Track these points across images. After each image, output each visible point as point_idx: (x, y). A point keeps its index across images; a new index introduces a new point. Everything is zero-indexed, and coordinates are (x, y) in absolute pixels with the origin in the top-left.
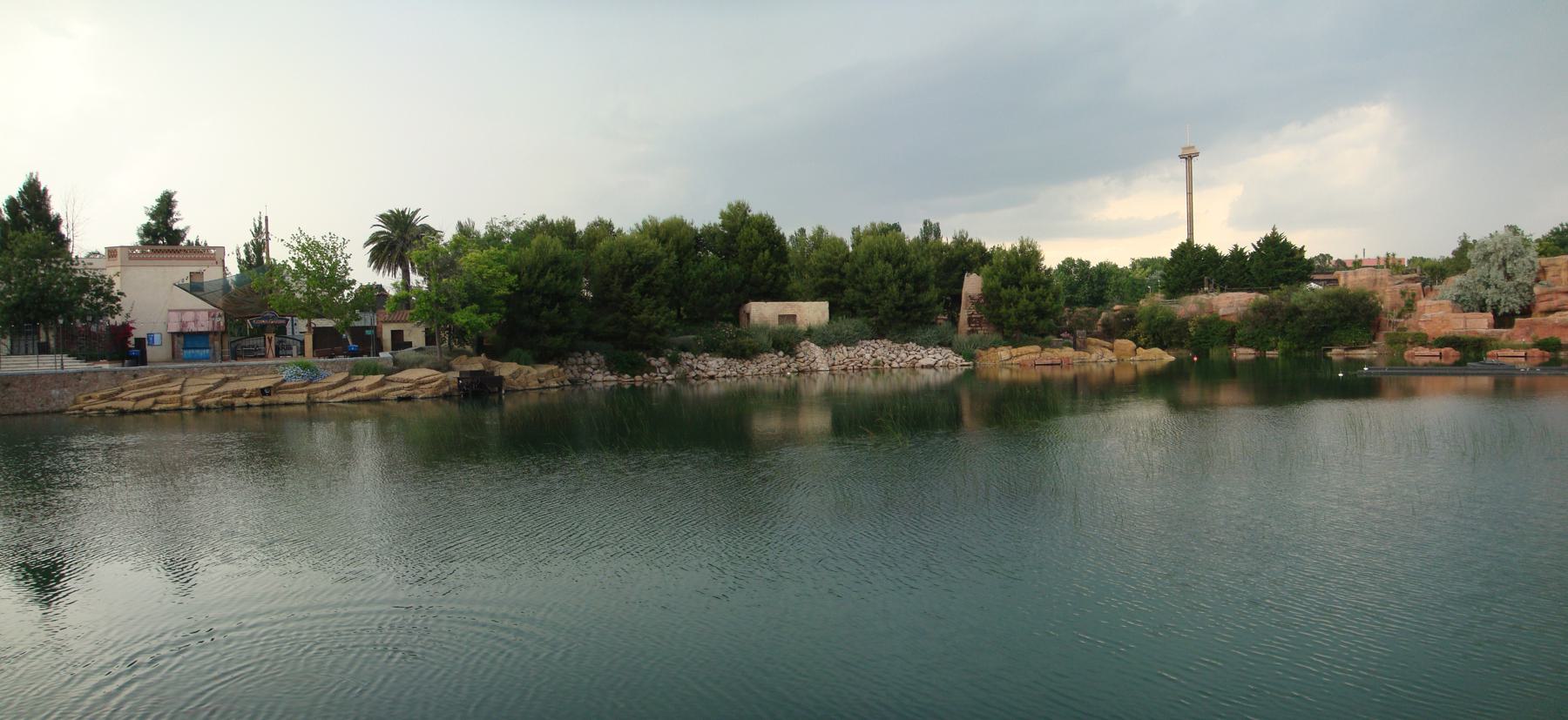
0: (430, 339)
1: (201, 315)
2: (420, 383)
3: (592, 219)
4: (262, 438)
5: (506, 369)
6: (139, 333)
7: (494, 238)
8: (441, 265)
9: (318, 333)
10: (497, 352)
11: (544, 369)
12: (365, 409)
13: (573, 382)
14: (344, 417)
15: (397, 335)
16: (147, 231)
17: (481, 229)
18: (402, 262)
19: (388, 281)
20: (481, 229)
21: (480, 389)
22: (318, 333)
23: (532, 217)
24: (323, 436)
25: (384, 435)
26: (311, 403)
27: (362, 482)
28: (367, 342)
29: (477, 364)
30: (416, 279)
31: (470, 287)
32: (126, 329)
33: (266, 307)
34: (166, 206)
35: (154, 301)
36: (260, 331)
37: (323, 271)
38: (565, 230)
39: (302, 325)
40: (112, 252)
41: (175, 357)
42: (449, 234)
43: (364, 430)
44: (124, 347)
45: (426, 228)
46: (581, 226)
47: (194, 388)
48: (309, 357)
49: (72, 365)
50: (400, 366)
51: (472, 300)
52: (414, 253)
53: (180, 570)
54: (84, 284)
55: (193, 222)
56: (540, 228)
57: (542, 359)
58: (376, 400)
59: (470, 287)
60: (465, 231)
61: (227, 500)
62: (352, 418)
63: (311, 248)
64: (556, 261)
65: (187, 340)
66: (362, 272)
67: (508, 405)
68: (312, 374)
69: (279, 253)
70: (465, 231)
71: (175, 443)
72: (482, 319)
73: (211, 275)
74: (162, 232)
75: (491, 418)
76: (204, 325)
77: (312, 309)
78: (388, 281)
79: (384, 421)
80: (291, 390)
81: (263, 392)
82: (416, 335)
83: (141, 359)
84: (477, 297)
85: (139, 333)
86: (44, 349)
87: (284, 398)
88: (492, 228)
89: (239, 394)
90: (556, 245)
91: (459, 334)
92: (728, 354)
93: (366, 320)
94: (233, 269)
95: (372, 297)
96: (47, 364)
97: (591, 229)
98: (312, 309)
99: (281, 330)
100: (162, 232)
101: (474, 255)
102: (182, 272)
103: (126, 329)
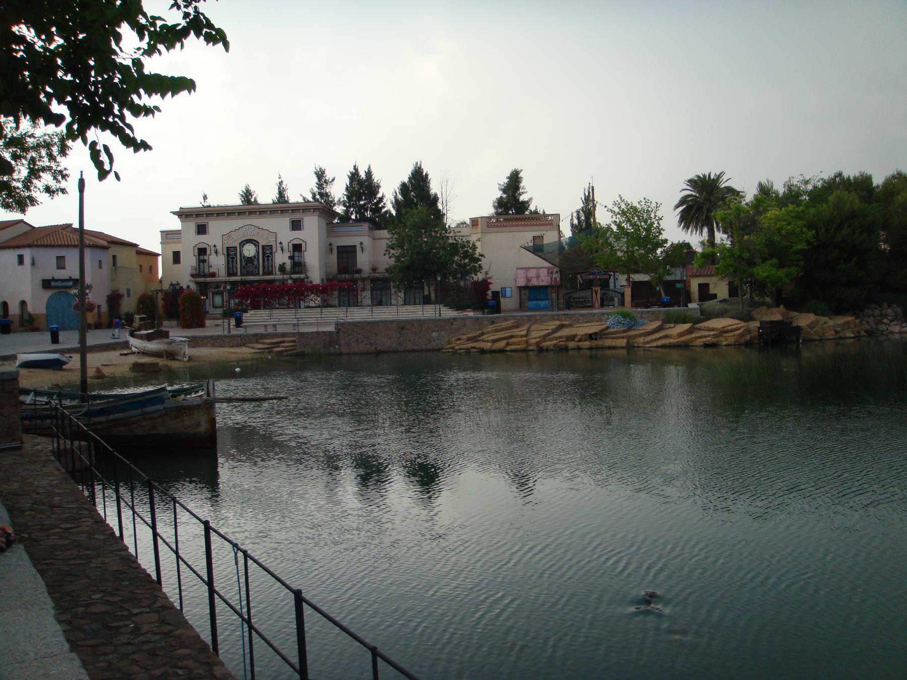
0: (733, 291)
1: (541, 272)
2: (723, 331)
3: (890, 172)
4: (589, 374)
5: (804, 320)
6: (495, 287)
7: (792, 195)
8: (744, 221)
9: (637, 287)
10: (796, 304)
11: (841, 320)
12: (675, 354)
13: (870, 333)
14: (658, 360)
15: (703, 288)
16: (501, 204)
17: (780, 188)
18: (708, 222)
19: (695, 239)
20: (780, 188)
21: (778, 338)
22: (637, 287)
23: (828, 174)
24: (639, 376)
25: (691, 378)
26: (630, 347)
27: (674, 419)
28: (677, 294)
29: (776, 315)
30: (720, 237)
31: (770, 243)
32: (485, 284)
33: (598, 263)
34: (514, 181)
35: (507, 262)
36: (588, 285)
37: (639, 228)
38: (864, 182)
39: (622, 279)
40: (474, 222)
41: (522, 307)
42: (750, 194)
43: (674, 374)
44: (483, 298)
45: (730, 190)
46: (878, 180)
47: (536, 334)
48: (628, 308)
49: (448, 313)
50: (707, 316)
51: (771, 255)
52: (719, 213)
53: (522, 481)
54: (455, 248)
55: (537, 196)
56: (837, 185)
57: (838, 310)
58: (685, 346)
59: (770, 243)
60: (765, 190)
61: (562, 426)
62: (665, 362)
63: (629, 212)
64: (853, 215)
65: (531, 293)
66: (673, 232)
67: (806, 354)
68: (631, 322)
69: (603, 218)
70: (765, 190)
71: (519, 376)
72: (781, 273)
73: (549, 238)
74: (512, 204)
75: (788, 366)
76: (544, 280)
77: (631, 265)
78: (695, 239)
79: (691, 364)
80: (612, 335)
81: (591, 337)
82: (721, 289)
83: (497, 309)
84: (776, 251)
85: (495, 287)
86: (427, 301)
87: (608, 342)
88: (790, 187)
89: (572, 338)
90: (853, 200)
91: (759, 286)
93: (677, 274)
94: (567, 232)
95: (682, 252)
96: (428, 312)
97: (889, 182)
98: (631, 265)
99: (605, 284)
100: (512, 204)
101: (773, 213)
102: (526, 236)
103: (485, 284)
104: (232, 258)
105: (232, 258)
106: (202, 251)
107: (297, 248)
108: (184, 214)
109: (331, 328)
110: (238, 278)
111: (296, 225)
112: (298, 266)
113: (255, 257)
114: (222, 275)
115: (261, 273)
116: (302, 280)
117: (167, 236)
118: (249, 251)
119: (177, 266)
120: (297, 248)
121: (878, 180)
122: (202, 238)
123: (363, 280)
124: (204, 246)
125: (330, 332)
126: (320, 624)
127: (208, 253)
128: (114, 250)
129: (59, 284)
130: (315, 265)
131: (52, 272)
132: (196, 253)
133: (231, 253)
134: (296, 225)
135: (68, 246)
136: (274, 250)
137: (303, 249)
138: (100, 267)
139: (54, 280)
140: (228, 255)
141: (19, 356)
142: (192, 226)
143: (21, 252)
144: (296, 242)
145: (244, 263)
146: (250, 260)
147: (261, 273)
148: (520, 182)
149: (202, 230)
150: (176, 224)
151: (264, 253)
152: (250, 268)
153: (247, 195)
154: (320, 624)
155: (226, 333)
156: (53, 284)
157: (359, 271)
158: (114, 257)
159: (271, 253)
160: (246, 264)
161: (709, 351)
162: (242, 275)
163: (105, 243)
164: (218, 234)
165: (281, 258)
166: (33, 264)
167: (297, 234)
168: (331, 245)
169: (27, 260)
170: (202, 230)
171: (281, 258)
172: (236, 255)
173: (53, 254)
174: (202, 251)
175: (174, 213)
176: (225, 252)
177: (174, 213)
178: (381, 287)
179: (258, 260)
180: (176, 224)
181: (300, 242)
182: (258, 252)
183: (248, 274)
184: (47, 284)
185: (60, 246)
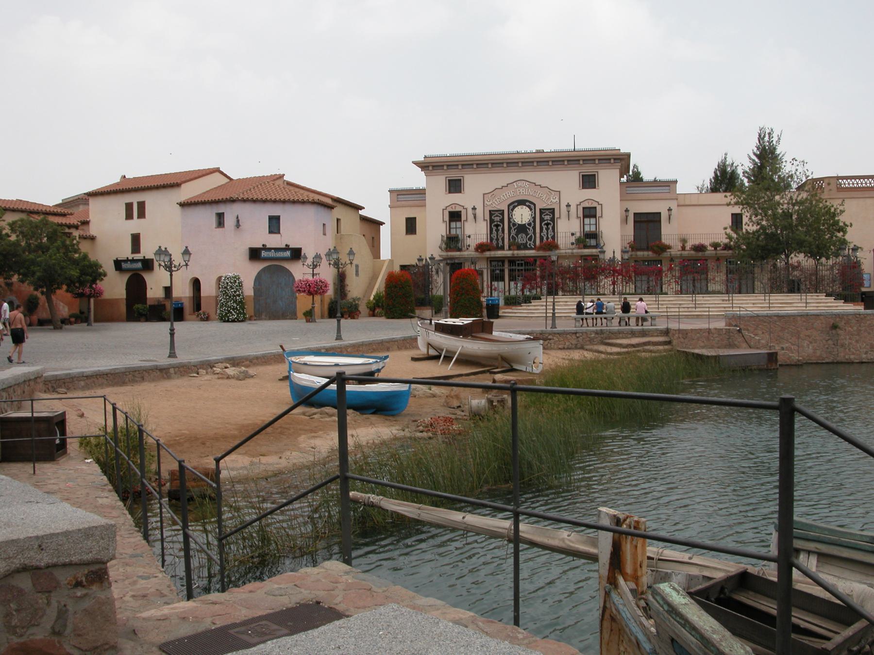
53: (182, 467)
92: (73, 504)
104: (497, 226)
105: (497, 226)
106: (455, 216)
107: (590, 213)
108: (429, 166)
109: (721, 325)
110: (507, 253)
111: (589, 182)
112: (590, 238)
113: (529, 224)
115: (506, 247)
116: (595, 258)
117: (401, 197)
118: (522, 215)
119: (411, 237)
120: (590, 213)
122: (455, 198)
123: (672, 259)
124: (458, 209)
125: (719, 330)
126: (171, 551)
127: (463, 218)
128: (339, 212)
129: (272, 254)
130: (615, 237)
131: (261, 237)
132: (447, 218)
133: (496, 219)
134: (589, 182)
135: (284, 202)
136: (557, 215)
138: (325, 234)
139: (265, 248)
140: (492, 221)
142: (440, 181)
143: (221, 209)
144: (586, 205)
145: (513, 233)
146: (522, 229)
147: (506, 247)
149: (455, 186)
150: (418, 179)
151: (542, 220)
152: (521, 239)
154: (171, 551)
155: (549, 329)
156: (264, 254)
157: (666, 248)
158: (338, 220)
159: (553, 219)
162: (510, 249)
163: (329, 201)
164: (477, 193)
166: (238, 225)
167: (589, 193)
168: (627, 211)
169: (229, 221)
170: (455, 186)
171: (567, 229)
172: (502, 221)
173: (265, 212)
174: (455, 216)
175: (415, 163)
176: (487, 217)
178: (695, 269)
179: (534, 228)
180: (418, 179)
182: (534, 218)
183: (519, 247)
184: (255, 254)
185: (275, 202)
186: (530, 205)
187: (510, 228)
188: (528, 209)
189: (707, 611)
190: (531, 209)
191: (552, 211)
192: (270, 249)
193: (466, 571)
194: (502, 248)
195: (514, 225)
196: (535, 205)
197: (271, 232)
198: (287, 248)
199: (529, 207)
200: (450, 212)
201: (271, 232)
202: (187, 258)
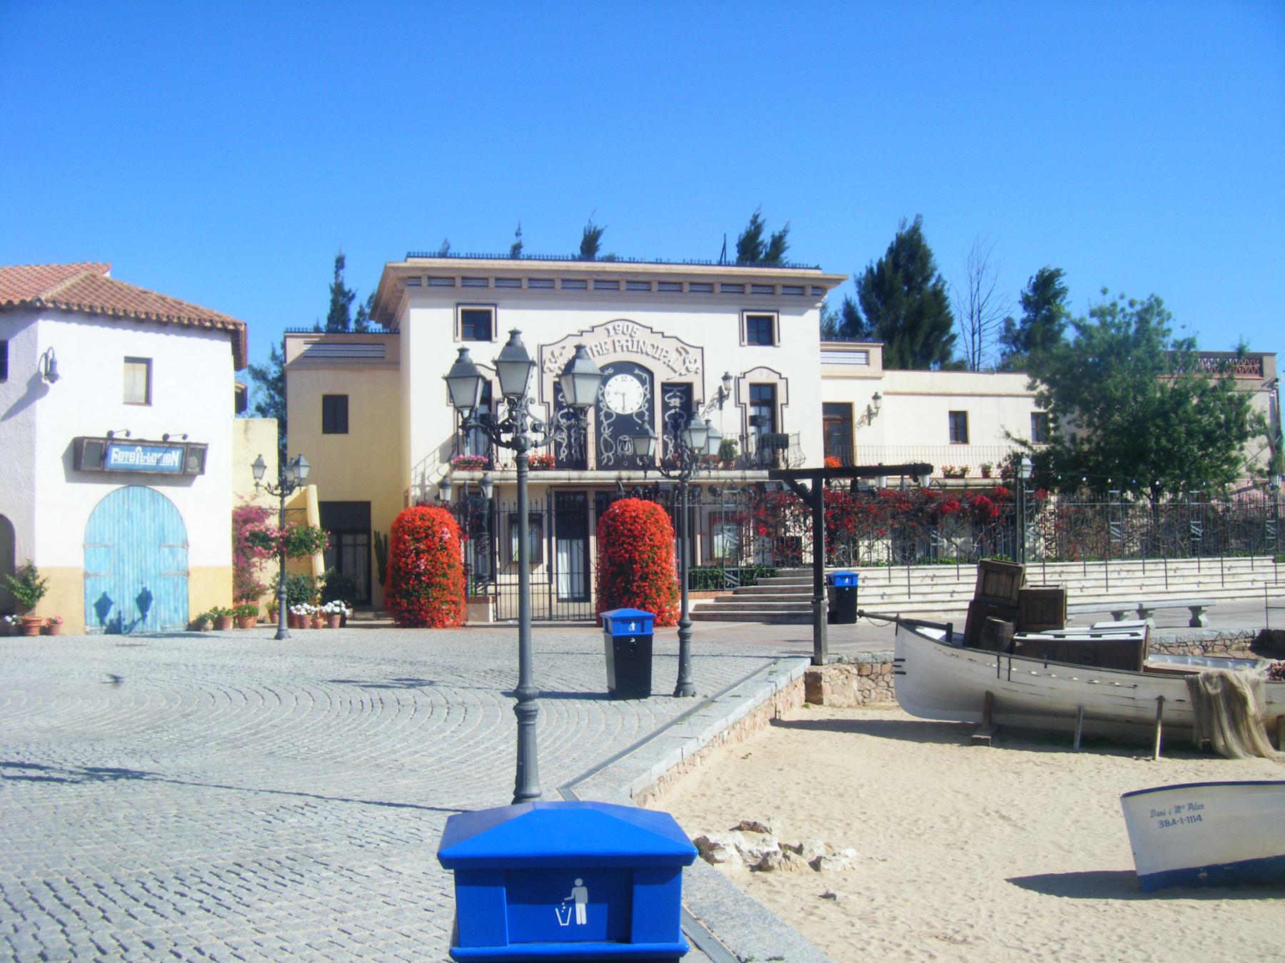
46: (684, 868)
111: (762, 332)
113: (641, 415)
114: (659, 455)
118: (625, 396)
120: (765, 396)
121: (684, 868)
129: (137, 458)
137: (781, 398)
141: (1265, 677)
144: (762, 377)
145: (606, 433)
147: (592, 462)
148: (782, 251)
153: (166, 437)
156: (118, 457)
160: (614, 435)
161: (173, 957)
162: (600, 467)
165: (726, 422)
171: (726, 422)
175: (785, 231)
177: (785, 231)
181: (772, 379)
182: (651, 402)
186: (644, 375)
187: (598, 424)
188: (636, 383)
189: (1049, 892)
190: (643, 382)
191: (686, 389)
192: (132, 444)
193: (98, 904)
194: (581, 465)
195: (608, 415)
196: (651, 374)
197: (344, 399)
198: (166, 444)
199: (639, 377)
200: (752, 386)
201: (344, 399)
202: (259, 473)
